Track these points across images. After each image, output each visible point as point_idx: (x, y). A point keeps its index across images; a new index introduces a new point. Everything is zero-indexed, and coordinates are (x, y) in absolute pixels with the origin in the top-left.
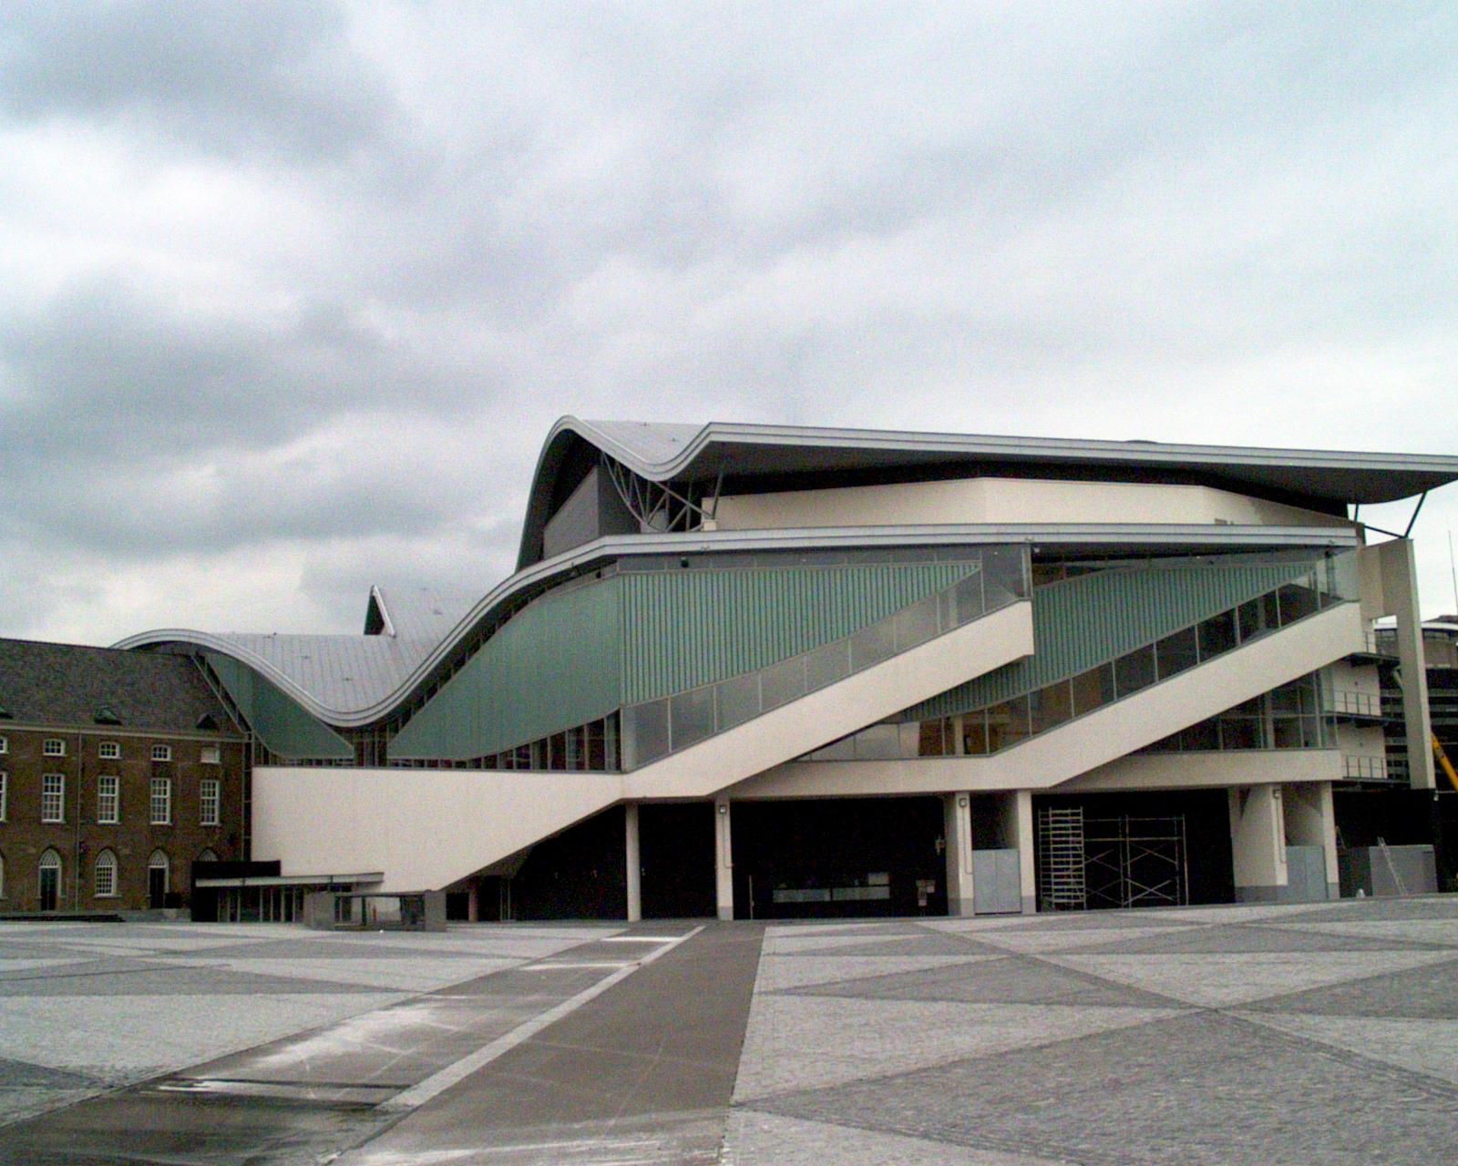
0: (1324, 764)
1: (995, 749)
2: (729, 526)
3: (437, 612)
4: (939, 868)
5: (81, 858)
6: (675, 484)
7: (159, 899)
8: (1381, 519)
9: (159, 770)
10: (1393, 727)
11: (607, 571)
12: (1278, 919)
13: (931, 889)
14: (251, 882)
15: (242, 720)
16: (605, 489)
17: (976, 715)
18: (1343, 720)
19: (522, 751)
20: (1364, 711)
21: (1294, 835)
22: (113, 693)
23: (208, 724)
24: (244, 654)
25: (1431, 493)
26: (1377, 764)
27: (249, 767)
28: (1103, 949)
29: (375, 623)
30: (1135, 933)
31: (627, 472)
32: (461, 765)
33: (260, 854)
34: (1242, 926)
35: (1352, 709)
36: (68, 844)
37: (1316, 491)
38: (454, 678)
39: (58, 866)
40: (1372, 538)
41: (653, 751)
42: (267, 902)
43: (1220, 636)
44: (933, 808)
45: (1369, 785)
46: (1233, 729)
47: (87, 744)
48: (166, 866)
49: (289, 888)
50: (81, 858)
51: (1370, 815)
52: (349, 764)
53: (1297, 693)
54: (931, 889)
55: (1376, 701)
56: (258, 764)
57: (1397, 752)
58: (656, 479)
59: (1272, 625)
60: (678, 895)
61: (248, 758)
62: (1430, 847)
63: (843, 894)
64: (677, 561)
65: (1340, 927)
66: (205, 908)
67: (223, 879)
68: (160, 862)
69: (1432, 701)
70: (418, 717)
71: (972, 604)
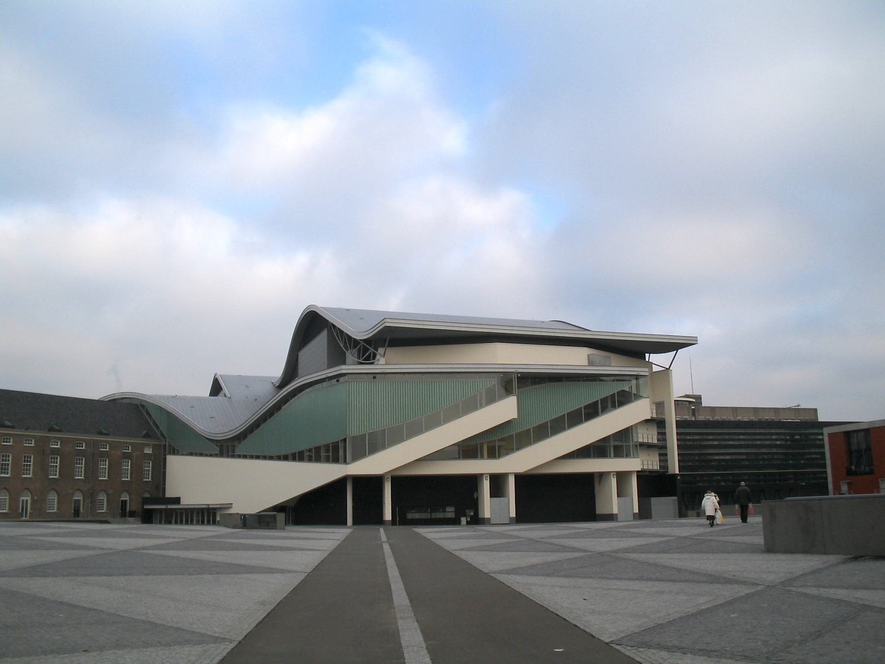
0: (633, 464)
1: (499, 457)
2: (387, 361)
3: (247, 387)
4: (474, 504)
5: (91, 496)
7: (124, 513)
8: (658, 360)
9: (127, 456)
10: (661, 448)
11: (342, 379)
12: (616, 527)
13: (472, 514)
14: (170, 507)
15: (162, 434)
16: (332, 341)
18: (642, 445)
20: (650, 441)
21: (621, 492)
23: (147, 436)
24: (171, 407)
26: (655, 463)
27: (165, 455)
28: (558, 537)
29: (216, 389)
30: (567, 532)
32: (271, 458)
33: (169, 494)
34: (604, 529)
35: (645, 441)
37: (635, 350)
38: (269, 420)
40: (655, 369)
41: (359, 455)
42: (177, 516)
43: (592, 412)
44: (473, 481)
45: (651, 472)
46: (597, 450)
47: (96, 444)
48: (128, 499)
49: (186, 509)
50: (91, 496)
51: (653, 485)
52: (216, 455)
53: (625, 434)
54: (472, 514)
55: (655, 437)
56: (170, 454)
57: (664, 458)
58: (358, 338)
60: (368, 514)
62: (676, 498)
64: (372, 376)
65: (637, 530)
66: (147, 517)
67: (154, 506)
68: (125, 497)
70: (250, 437)
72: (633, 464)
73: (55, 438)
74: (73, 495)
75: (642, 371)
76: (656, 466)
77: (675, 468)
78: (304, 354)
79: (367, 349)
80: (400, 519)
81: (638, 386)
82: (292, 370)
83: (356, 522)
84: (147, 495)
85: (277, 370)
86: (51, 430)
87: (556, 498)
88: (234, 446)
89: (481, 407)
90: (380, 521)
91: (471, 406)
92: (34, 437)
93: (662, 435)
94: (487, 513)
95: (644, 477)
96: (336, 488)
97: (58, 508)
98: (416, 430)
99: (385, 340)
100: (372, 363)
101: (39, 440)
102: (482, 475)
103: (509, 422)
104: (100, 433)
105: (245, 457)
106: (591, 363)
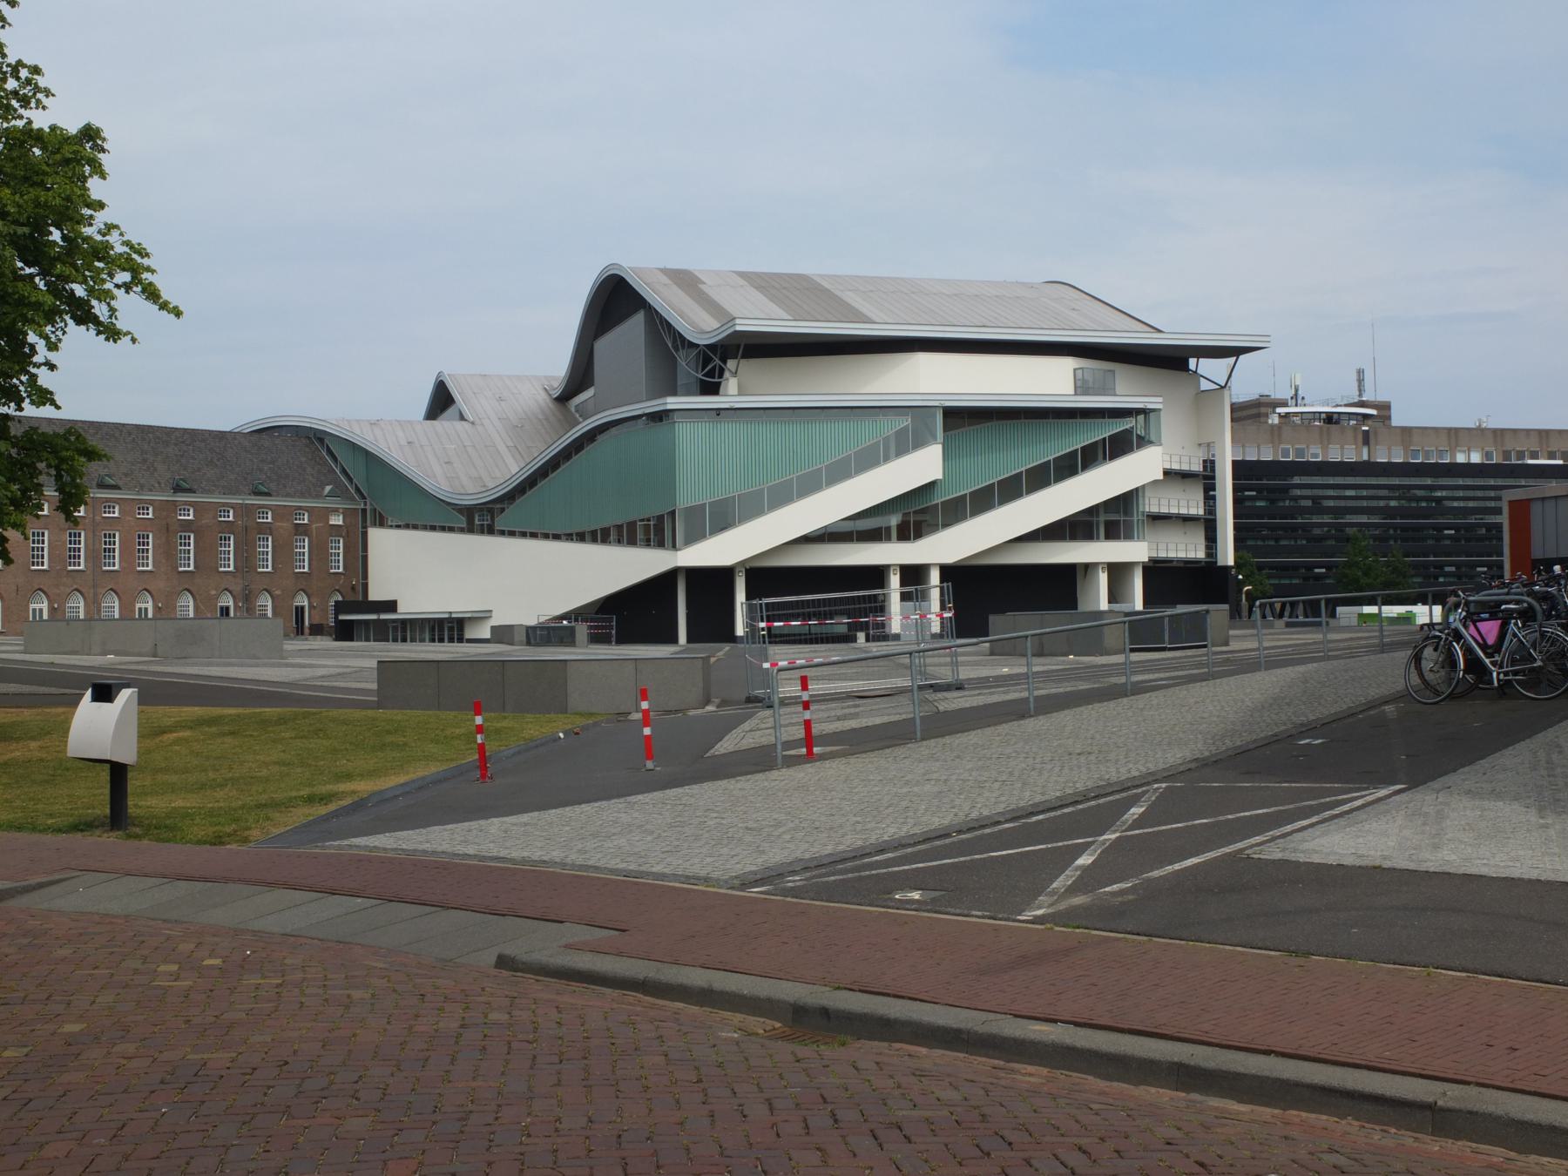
0: (1135, 551)
3: (501, 399)
5: (247, 600)
6: (712, 347)
9: (301, 530)
14: (384, 616)
15: (358, 490)
17: (915, 514)
22: (261, 470)
27: (365, 527)
29: (441, 401)
32: (557, 537)
33: (374, 596)
36: (237, 589)
39: (231, 604)
40: (1205, 385)
41: (695, 536)
43: (1067, 467)
44: (875, 576)
49: (404, 622)
50: (247, 600)
52: (462, 530)
56: (374, 525)
61: (364, 520)
62: (1226, 607)
66: (345, 632)
71: (905, 444)
72: (1135, 551)
73: (186, 503)
74: (217, 597)
76: (1201, 554)
77: (1227, 555)
78: (602, 346)
82: (581, 374)
83: (690, 640)
85: (558, 365)
86: (178, 489)
89: (887, 459)
90: (731, 637)
91: (868, 460)
92: (151, 502)
94: (895, 626)
95: (1156, 572)
96: (659, 588)
98: (781, 496)
99: (738, 346)
101: (161, 507)
102: (888, 567)
103: (932, 484)
105: (512, 534)
106: (1081, 388)
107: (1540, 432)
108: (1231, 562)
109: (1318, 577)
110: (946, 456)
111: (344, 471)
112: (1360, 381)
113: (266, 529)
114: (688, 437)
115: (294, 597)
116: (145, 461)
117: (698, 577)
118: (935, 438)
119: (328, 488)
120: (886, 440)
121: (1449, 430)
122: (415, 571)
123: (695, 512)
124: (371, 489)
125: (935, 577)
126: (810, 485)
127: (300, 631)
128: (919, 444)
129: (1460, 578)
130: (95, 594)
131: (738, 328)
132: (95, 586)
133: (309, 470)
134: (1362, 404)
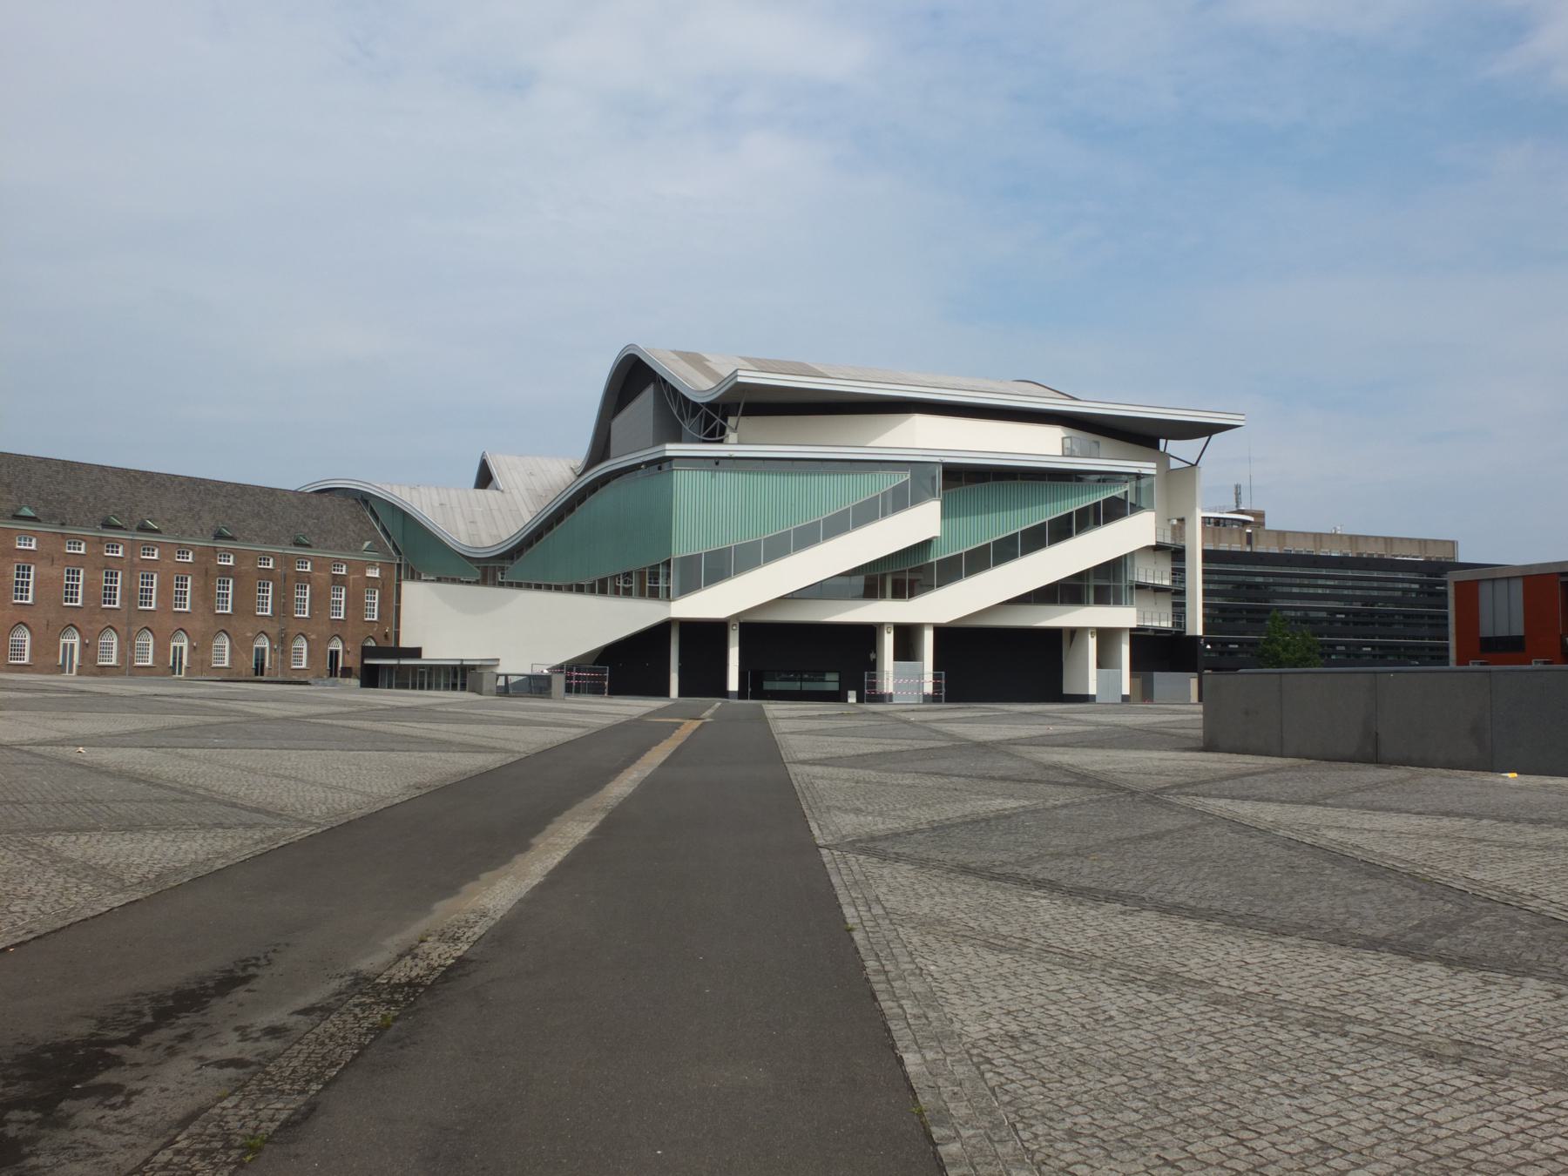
0: (1123, 617)
1: (912, 596)
5: (283, 642)
6: (708, 405)
8: (1180, 450)
9: (338, 581)
10: (1177, 594)
16: (659, 397)
17: (904, 573)
18: (1141, 587)
19: (603, 582)
21: (1105, 660)
25: (1214, 437)
27: (399, 580)
31: (675, 391)
32: (558, 588)
33: (403, 644)
36: (273, 631)
39: (267, 646)
40: (1174, 464)
41: (690, 586)
43: (1062, 530)
44: (868, 634)
49: (431, 667)
51: (1158, 652)
52: (477, 583)
56: (407, 578)
57: (1179, 610)
59: (1097, 524)
60: (704, 678)
63: (808, 686)
66: (371, 678)
68: (337, 645)
69: (1205, 572)
71: (900, 501)
72: (1123, 617)
73: (226, 549)
75: (1148, 467)
76: (1166, 624)
77: (1196, 625)
78: (617, 424)
79: (712, 417)
80: (753, 686)
81: (1138, 490)
82: (601, 449)
83: (681, 694)
84: (372, 643)
86: (219, 536)
87: (1001, 663)
88: (502, 569)
89: (884, 515)
90: (722, 692)
91: (867, 513)
92: (192, 548)
93: (1179, 573)
94: (888, 684)
95: (1141, 639)
97: (231, 660)
98: (778, 548)
100: (721, 442)
102: (882, 625)
104: (298, 544)
107: (1385, 539)
108: (1200, 632)
109: (1232, 653)
110: (945, 514)
111: (384, 530)
112: (1238, 494)
113: (303, 579)
114: (685, 483)
115: (329, 642)
116: (191, 509)
117: (692, 629)
118: (933, 495)
119: (367, 544)
120: (884, 494)
121: (1315, 535)
122: (436, 621)
123: (690, 562)
124: (414, 549)
125: (928, 637)
126: (807, 537)
127: (333, 672)
128: (917, 500)
129: (1348, 656)
130: (129, 633)
131: (740, 379)
132: (130, 624)
133: (352, 527)
134: (1242, 512)
